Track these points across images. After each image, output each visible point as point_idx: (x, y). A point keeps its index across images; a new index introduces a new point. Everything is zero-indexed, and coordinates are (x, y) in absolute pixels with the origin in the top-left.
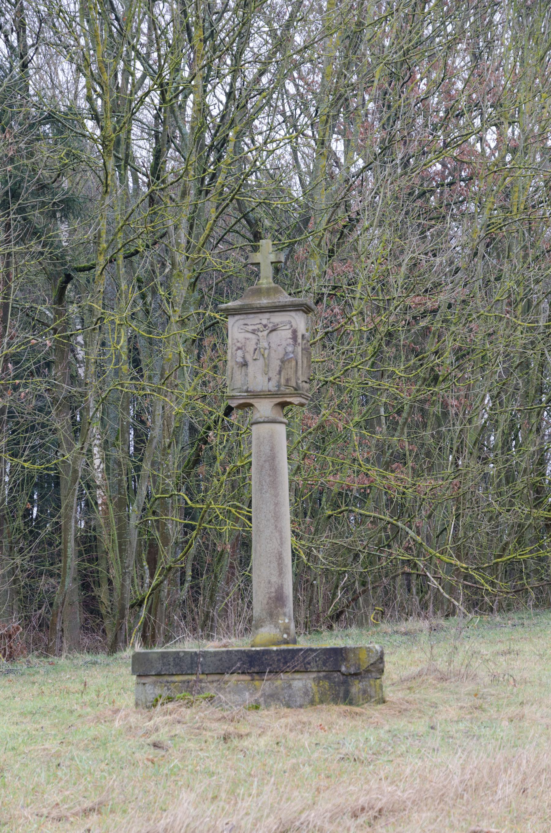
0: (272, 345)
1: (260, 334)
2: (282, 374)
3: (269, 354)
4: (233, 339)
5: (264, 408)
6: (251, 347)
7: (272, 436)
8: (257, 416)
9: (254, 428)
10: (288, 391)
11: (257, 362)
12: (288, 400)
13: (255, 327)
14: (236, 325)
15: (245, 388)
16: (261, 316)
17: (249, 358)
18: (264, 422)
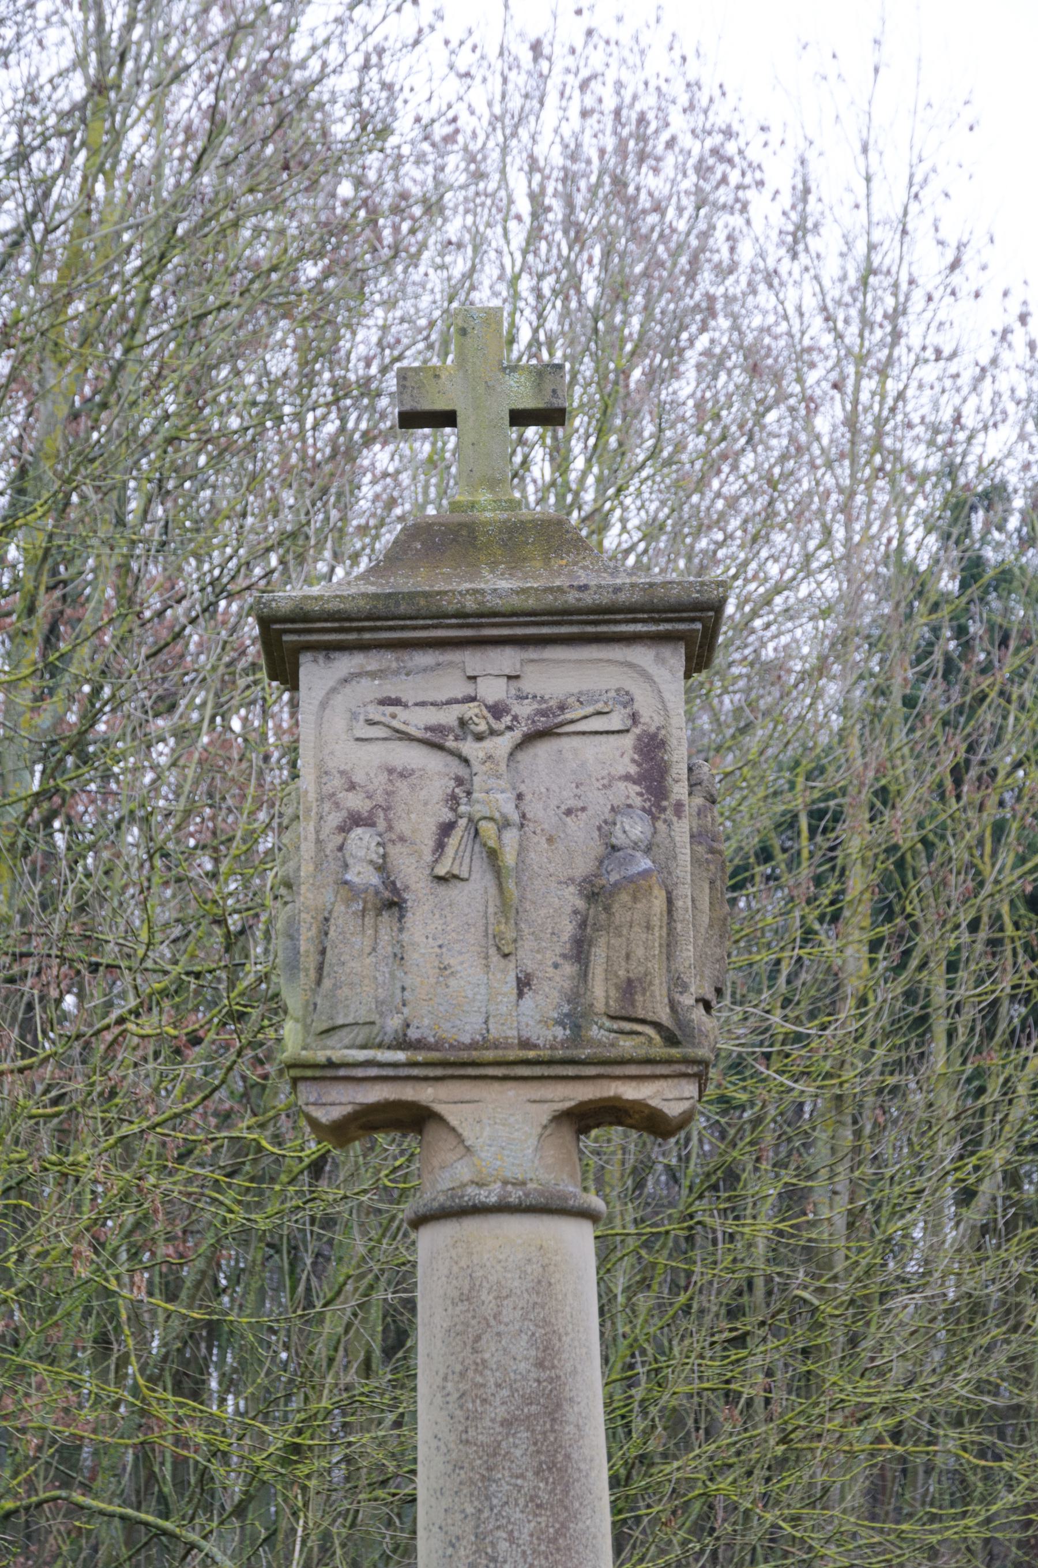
0: (534, 809)
1: (469, 748)
2: (599, 955)
3: (522, 849)
4: (323, 773)
5: (501, 1133)
6: (421, 813)
7: (543, 1286)
8: (446, 1174)
9: (432, 1243)
10: (627, 1046)
11: (454, 892)
12: (630, 1092)
13: (448, 717)
14: (339, 701)
15: (394, 1023)
16: (473, 660)
17: (411, 871)
18: (503, 1208)
